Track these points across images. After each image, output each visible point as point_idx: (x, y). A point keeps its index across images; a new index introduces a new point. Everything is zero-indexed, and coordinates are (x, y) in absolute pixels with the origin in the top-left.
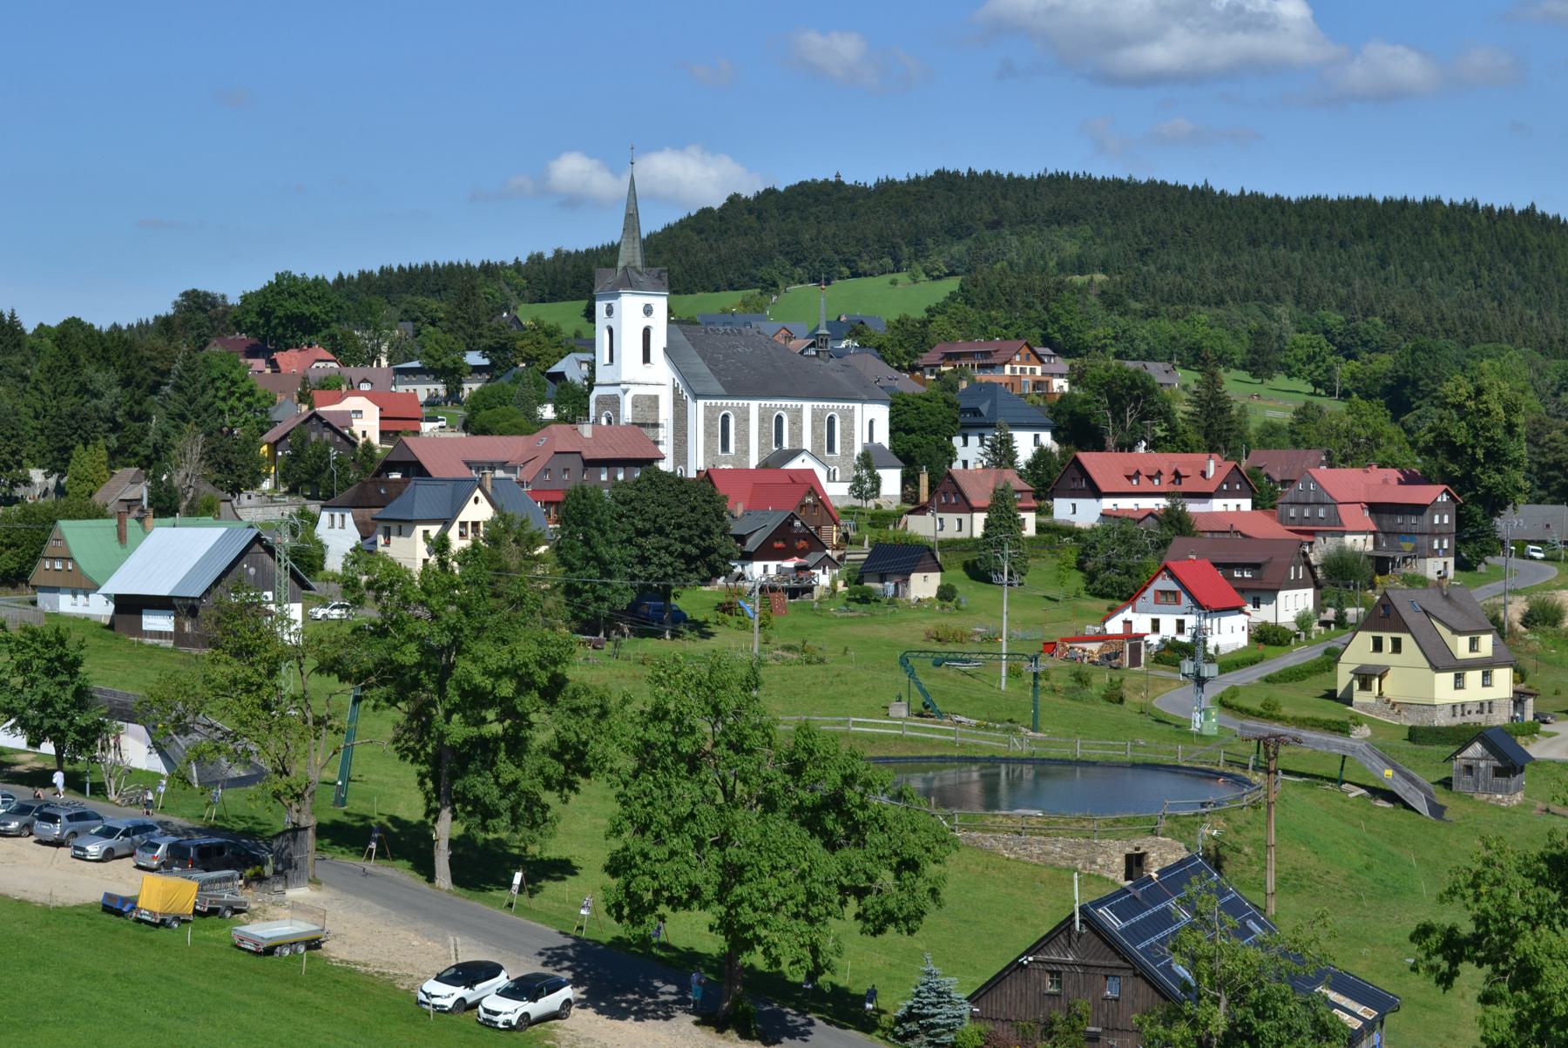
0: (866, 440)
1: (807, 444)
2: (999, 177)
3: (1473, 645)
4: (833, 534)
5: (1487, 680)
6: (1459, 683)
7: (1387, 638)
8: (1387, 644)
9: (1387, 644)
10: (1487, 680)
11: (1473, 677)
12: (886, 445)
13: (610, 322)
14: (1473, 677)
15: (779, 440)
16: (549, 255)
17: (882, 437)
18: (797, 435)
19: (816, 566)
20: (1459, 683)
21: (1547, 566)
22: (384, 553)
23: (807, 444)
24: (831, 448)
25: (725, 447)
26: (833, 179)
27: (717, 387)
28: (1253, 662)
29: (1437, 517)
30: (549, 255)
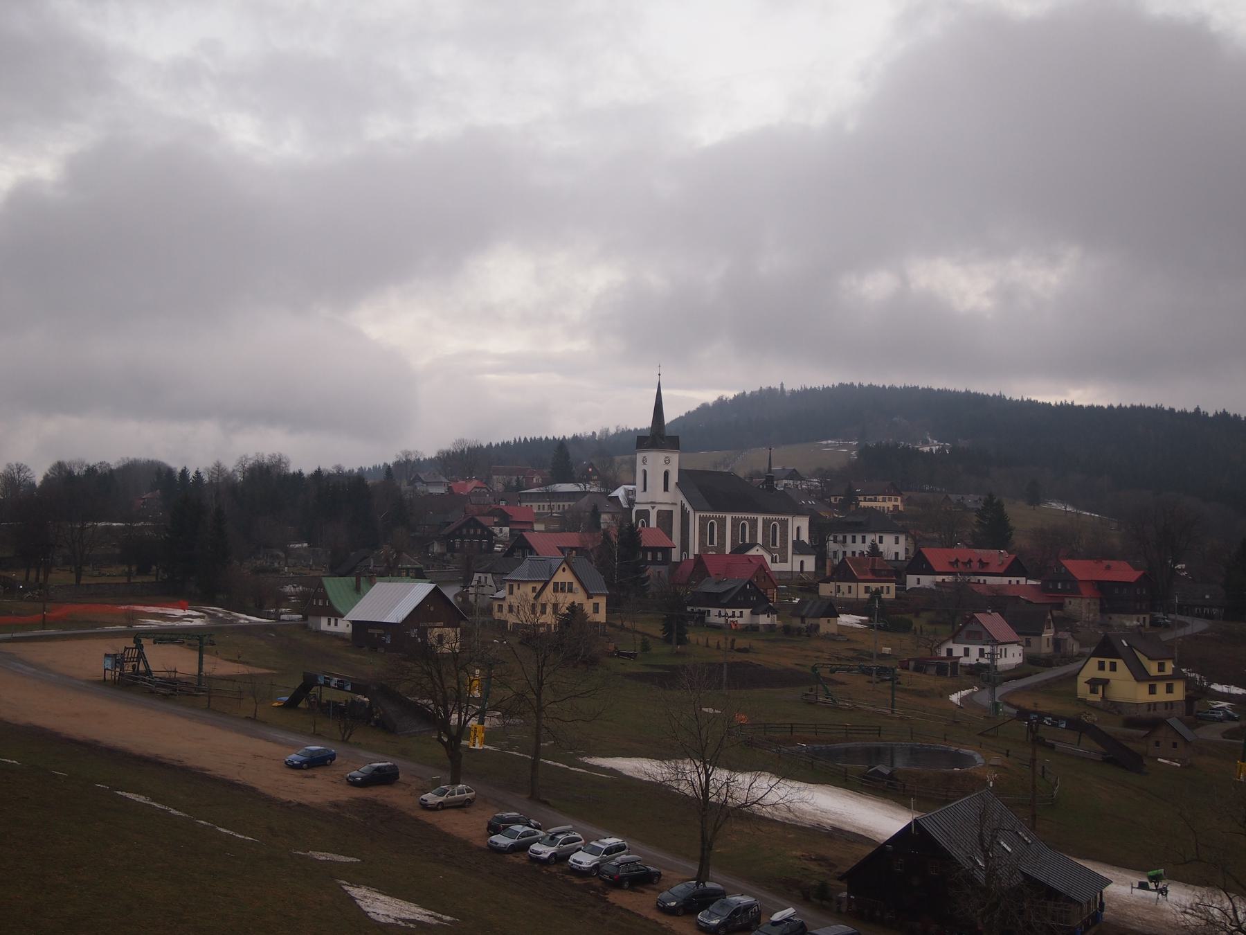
0: (795, 539)
7: (1107, 661)
8: (541, 508)
9: (541, 508)
10: (1169, 690)
11: (1161, 687)
14: (1161, 687)
16: (639, 429)
17: (805, 537)
23: (760, 541)
25: (712, 542)
26: (779, 387)
30: (639, 429)
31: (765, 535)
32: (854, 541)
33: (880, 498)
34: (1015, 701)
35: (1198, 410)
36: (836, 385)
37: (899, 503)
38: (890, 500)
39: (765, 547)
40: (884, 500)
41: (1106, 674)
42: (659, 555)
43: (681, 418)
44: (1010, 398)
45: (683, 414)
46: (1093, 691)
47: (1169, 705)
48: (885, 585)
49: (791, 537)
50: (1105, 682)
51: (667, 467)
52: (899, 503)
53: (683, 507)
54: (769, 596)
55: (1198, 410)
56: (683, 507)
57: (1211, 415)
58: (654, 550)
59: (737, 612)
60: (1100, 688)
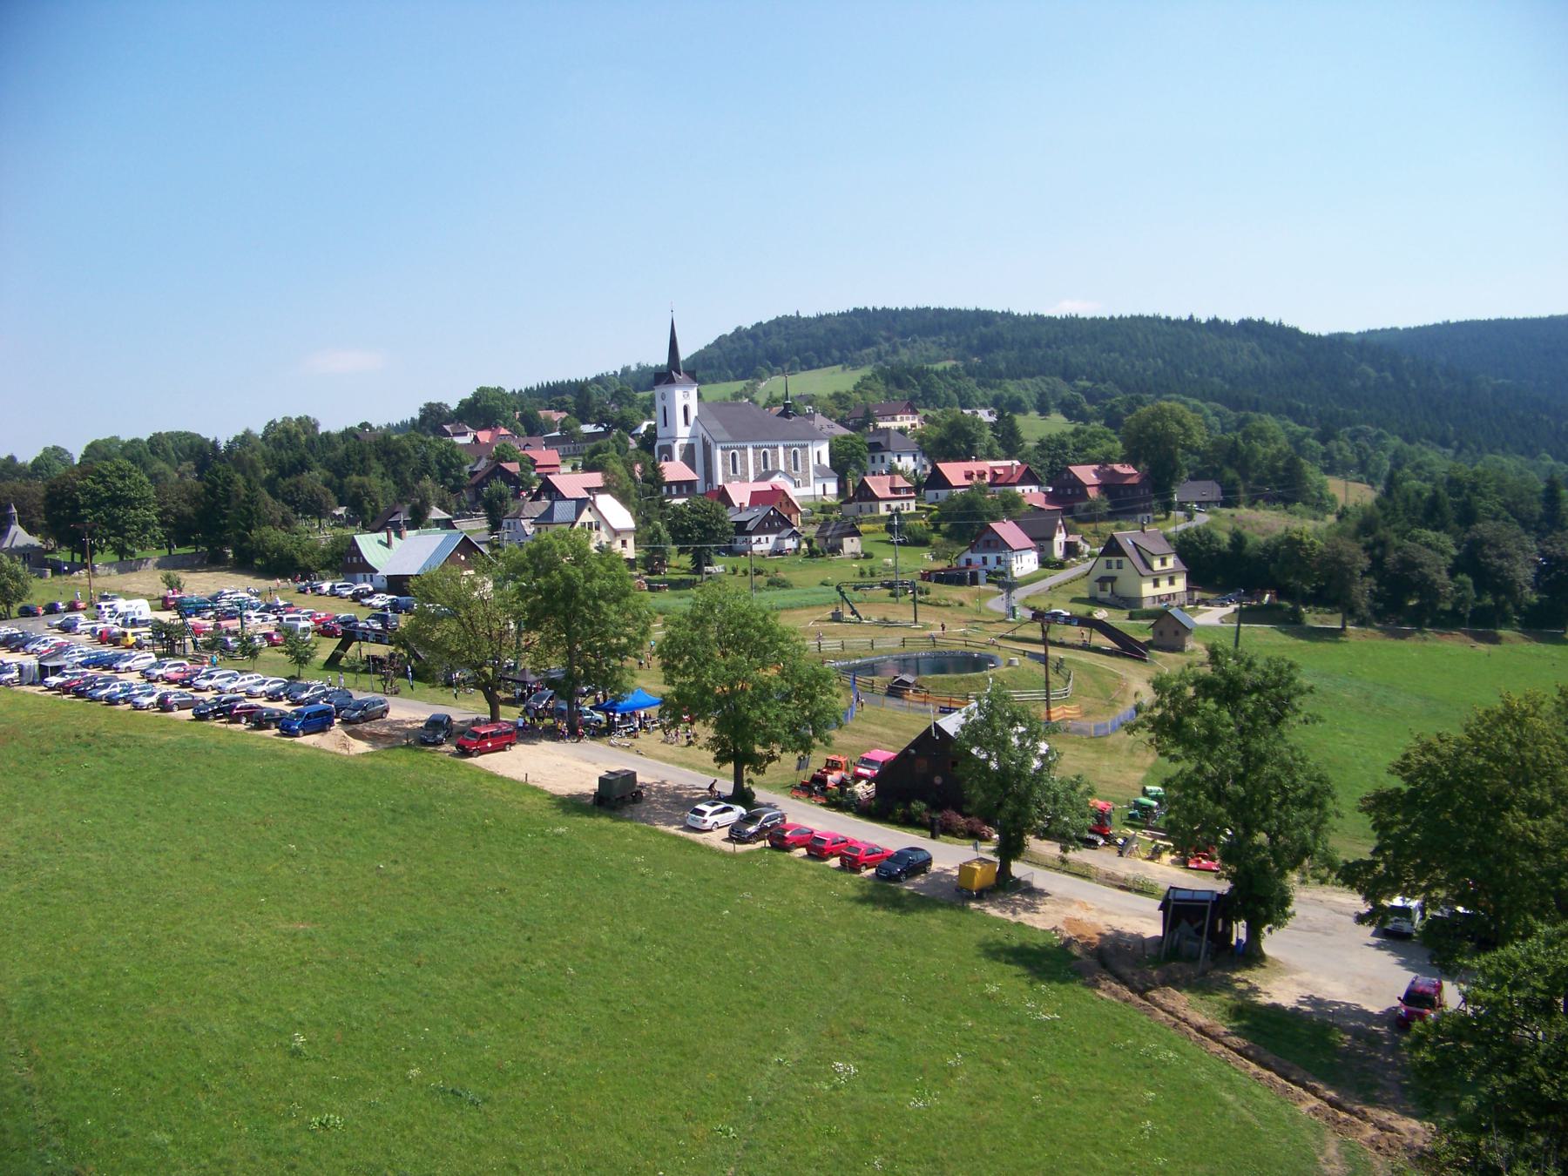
0: (816, 462)
1: (782, 467)
2: (890, 311)
3: (1163, 562)
4: (796, 519)
5: (1172, 582)
6: (1156, 584)
7: (1114, 560)
8: (1114, 564)
9: (1114, 564)
10: (1172, 582)
11: (1164, 583)
12: (828, 465)
13: (664, 403)
14: (1164, 583)
15: (766, 466)
16: (634, 368)
17: (826, 461)
18: (776, 462)
19: (788, 537)
20: (1156, 584)
21: (842, 876)
22: (1501, 568)
23: (782, 467)
24: (796, 468)
25: (735, 471)
26: (794, 314)
27: (726, 436)
28: (1045, 577)
29: (1229, 833)
30: (634, 368)
31: (787, 463)
32: (873, 461)
33: (898, 417)
34: (1031, 603)
35: (1191, 317)
36: (851, 309)
37: (916, 421)
38: (908, 419)
39: (786, 474)
40: (902, 419)
41: (1114, 572)
42: (674, 488)
43: (700, 351)
44: (638, 365)
45: (947, 308)
46: (1103, 589)
47: (1173, 596)
48: (905, 502)
49: (812, 461)
50: (1113, 579)
51: (685, 402)
52: (916, 421)
53: (704, 440)
54: (793, 521)
55: (1191, 317)
56: (704, 440)
57: (1204, 321)
58: (679, 484)
59: (763, 538)
60: (1109, 585)
